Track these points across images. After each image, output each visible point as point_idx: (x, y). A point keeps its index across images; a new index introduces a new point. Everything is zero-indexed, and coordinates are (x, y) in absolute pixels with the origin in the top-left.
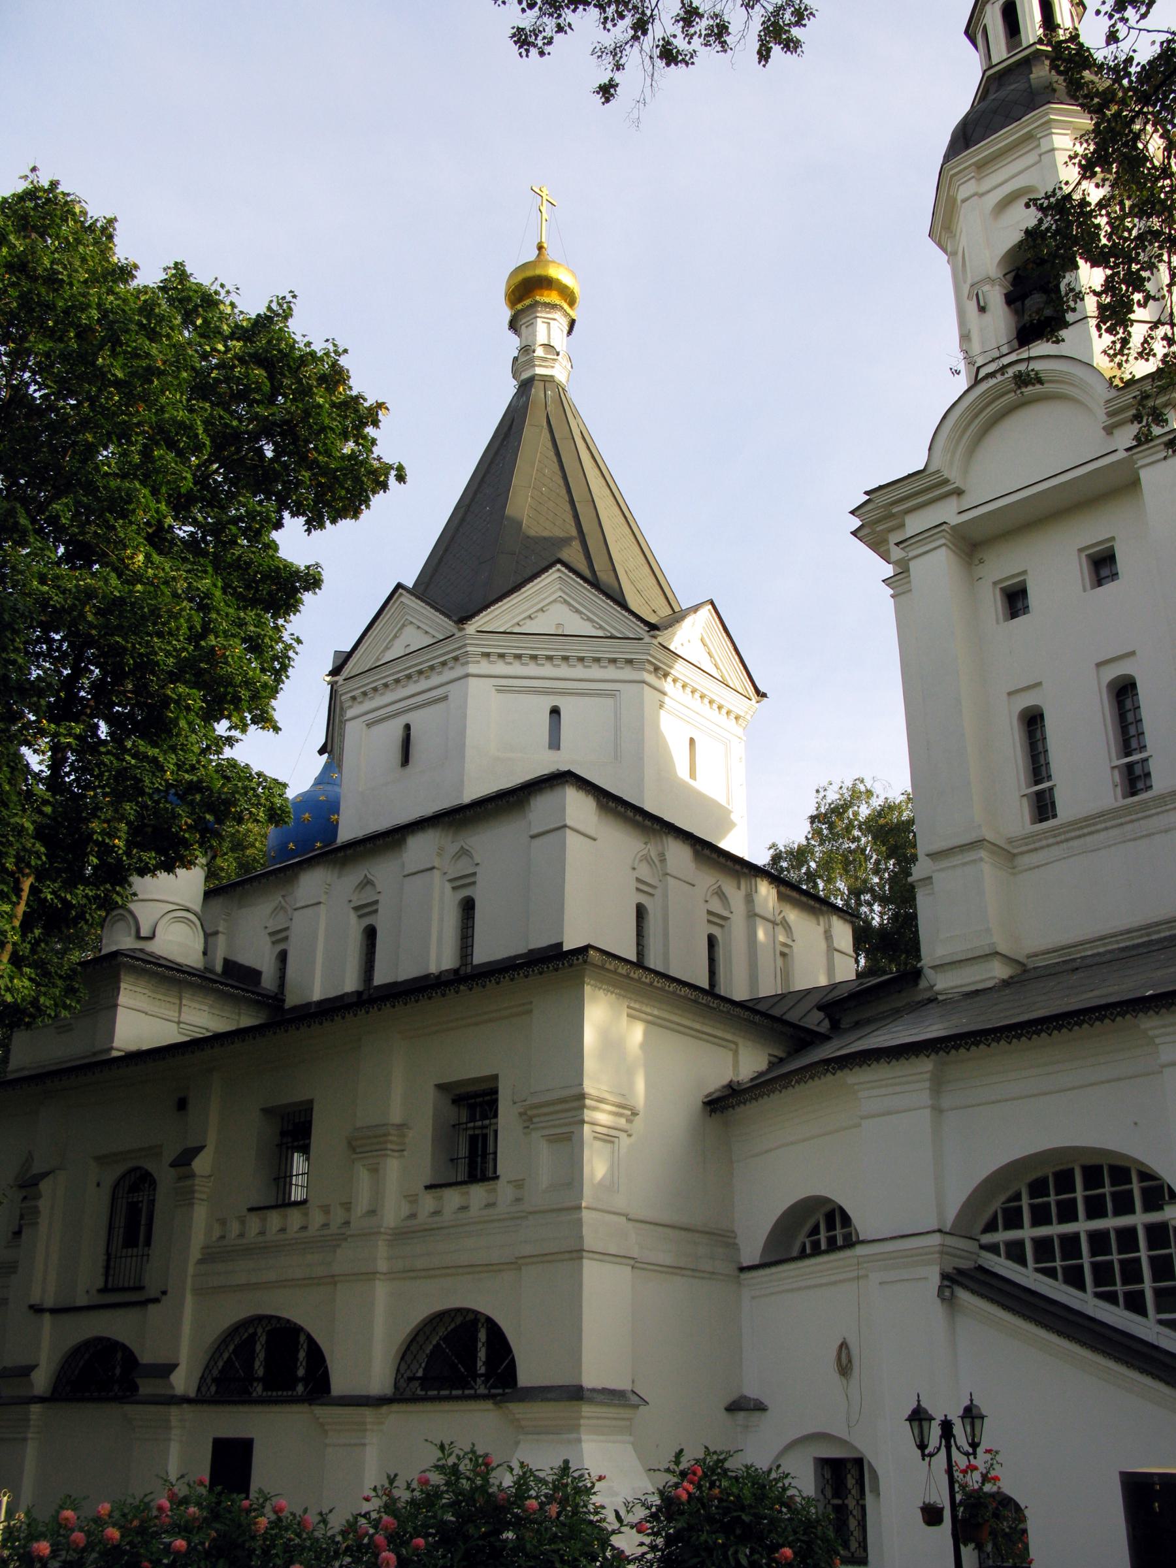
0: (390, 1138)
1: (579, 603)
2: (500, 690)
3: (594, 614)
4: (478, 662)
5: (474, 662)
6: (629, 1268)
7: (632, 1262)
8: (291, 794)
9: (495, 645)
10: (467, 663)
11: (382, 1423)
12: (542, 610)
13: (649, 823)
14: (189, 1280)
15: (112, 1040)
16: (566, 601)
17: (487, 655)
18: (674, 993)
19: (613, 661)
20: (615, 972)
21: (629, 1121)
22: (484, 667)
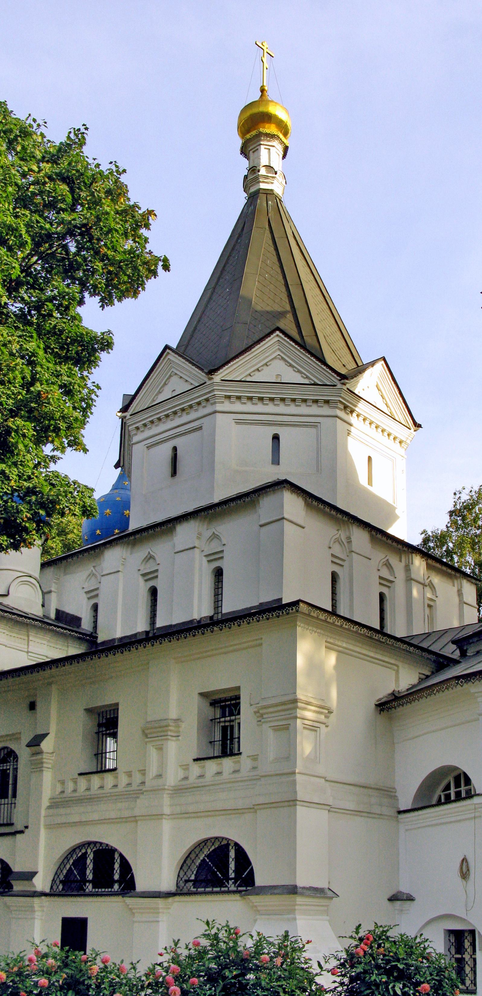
0: (170, 728)
1: (292, 360)
2: (239, 422)
4: (223, 402)
5: (220, 403)
10: (215, 403)
11: (169, 908)
17: (229, 397)
18: (356, 632)
22: (226, 406)
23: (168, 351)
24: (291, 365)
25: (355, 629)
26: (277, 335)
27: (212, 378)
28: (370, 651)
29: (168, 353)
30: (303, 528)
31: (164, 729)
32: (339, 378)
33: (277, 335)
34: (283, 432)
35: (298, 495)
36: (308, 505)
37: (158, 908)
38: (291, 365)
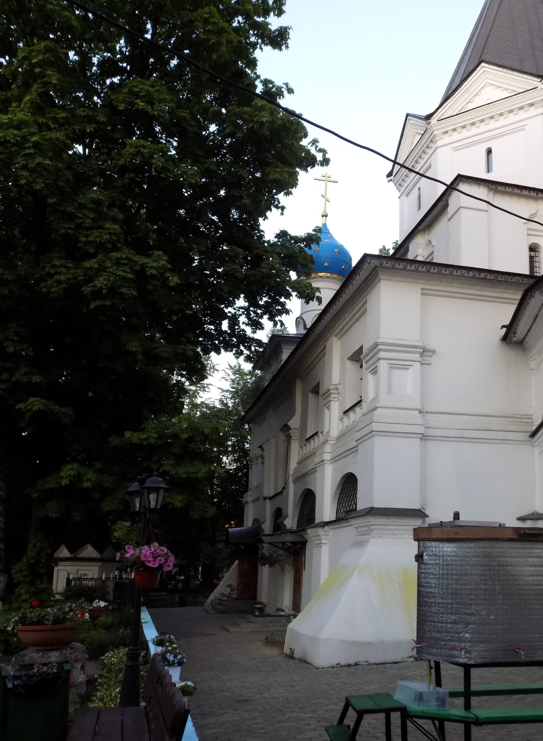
0: (331, 391)
1: (499, 82)
2: (456, 149)
3: (508, 84)
4: (442, 138)
5: (440, 139)
6: (419, 439)
7: (421, 436)
8: (261, 220)
9: (448, 125)
10: (436, 141)
11: (328, 535)
12: (476, 95)
13: (510, 190)
14: (291, 477)
15: (331, 381)
16: (491, 84)
17: (446, 132)
18: (474, 277)
19: (521, 108)
20: (462, 276)
21: (421, 355)
22: (447, 139)
23: (409, 117)
24: (499, 87)
25: (524, 282)
26: (483, 67)
27: (430, 122)
28: (460, 288)
29: (410, 119)
30: (487, 211)
31: (327, 394)
32: (539, 80)
33: (483, 67)
34: (494, 145)
35: (479, 184)
36: (490, 189)
37: (319, 536)
38: (499, 87)
